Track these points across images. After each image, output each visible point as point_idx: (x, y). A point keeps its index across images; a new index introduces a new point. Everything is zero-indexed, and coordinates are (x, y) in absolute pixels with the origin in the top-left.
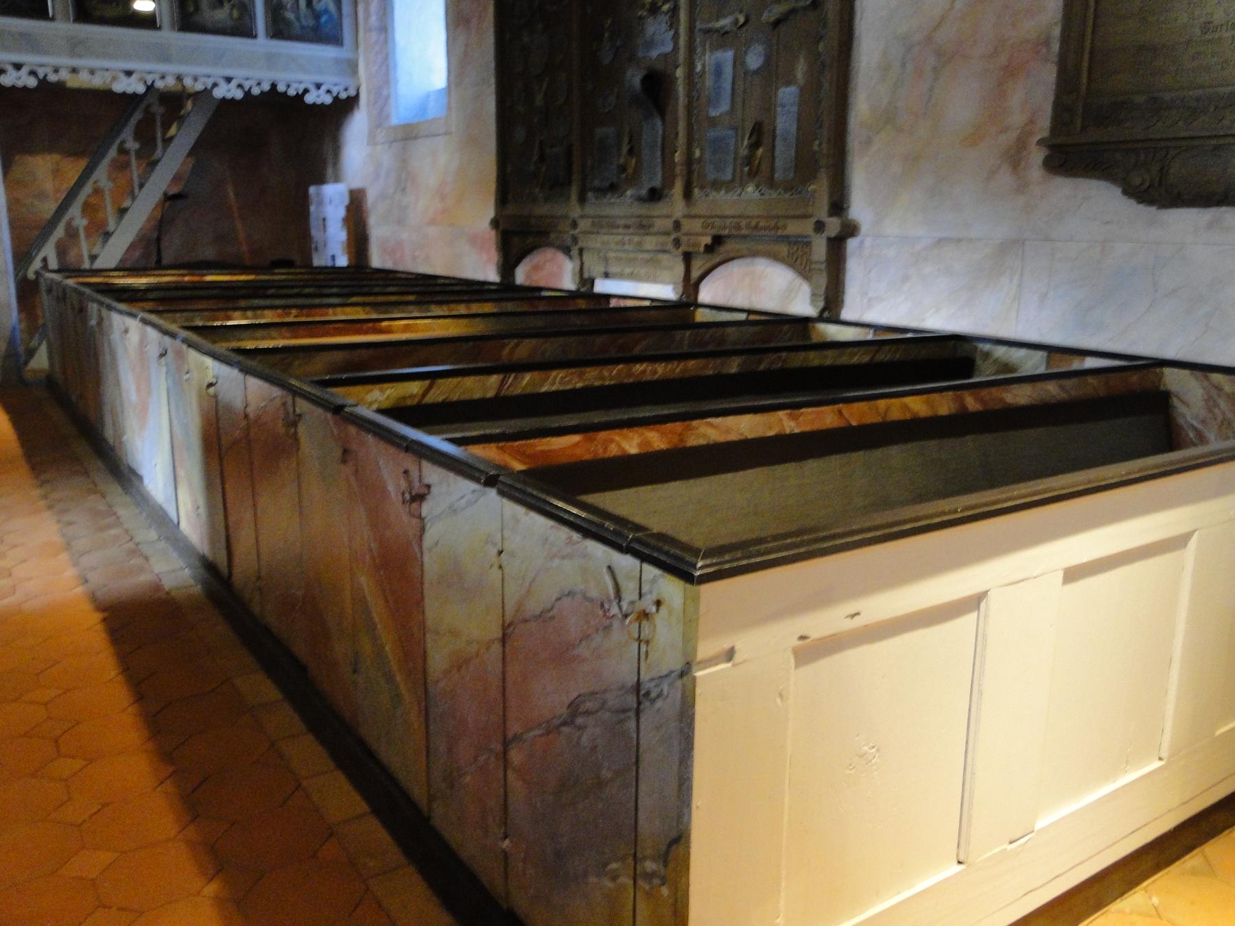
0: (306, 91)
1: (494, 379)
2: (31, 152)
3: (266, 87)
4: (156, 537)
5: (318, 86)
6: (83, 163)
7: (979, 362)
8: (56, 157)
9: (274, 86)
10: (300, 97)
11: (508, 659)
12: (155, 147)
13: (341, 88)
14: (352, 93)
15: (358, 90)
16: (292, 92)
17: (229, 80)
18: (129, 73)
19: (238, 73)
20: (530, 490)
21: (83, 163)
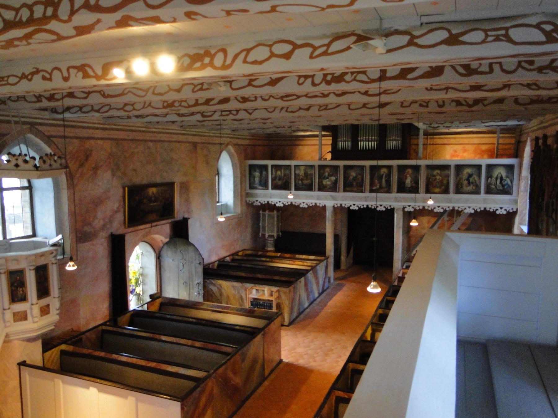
0: (497, 210)
1: (155, 363)
2: (423, 216)
3: (482, 209)
4: (64, 76)
5: (501, 208)
6: (436, 219)
7: (381, 122)
8: (430, 217)
9: (485, 209)
10: (275, 205)
11: (410, 88)
12: (453, 217)
13: (510, 209)
14: (515, 210)
15: (517, 209)
16: (491, 210)
17: (469, 207)
18: (439, 207)
19: (384, 204)
20: (192, 130)
21: (436, 219)
